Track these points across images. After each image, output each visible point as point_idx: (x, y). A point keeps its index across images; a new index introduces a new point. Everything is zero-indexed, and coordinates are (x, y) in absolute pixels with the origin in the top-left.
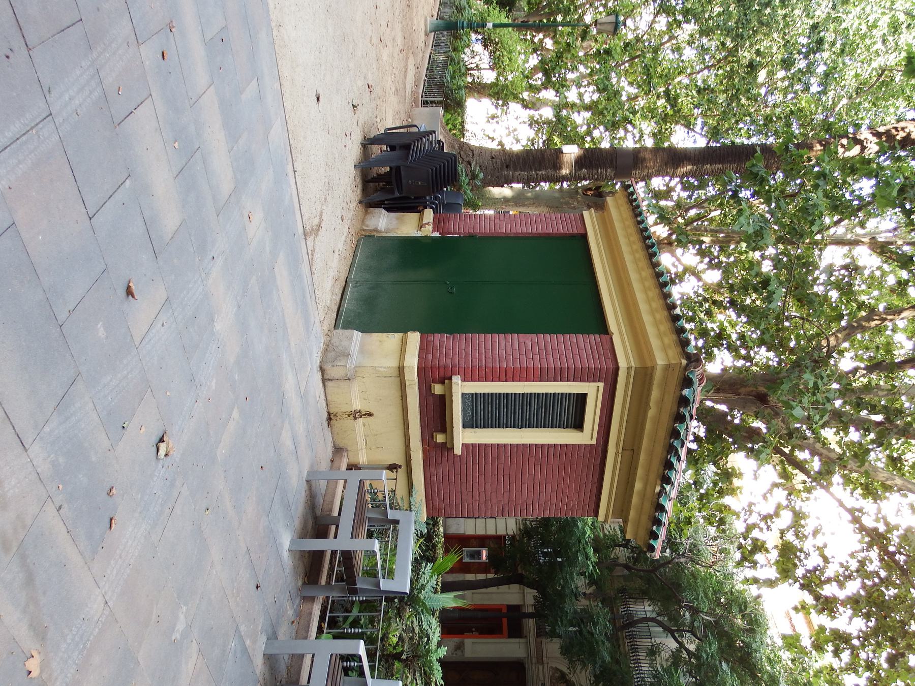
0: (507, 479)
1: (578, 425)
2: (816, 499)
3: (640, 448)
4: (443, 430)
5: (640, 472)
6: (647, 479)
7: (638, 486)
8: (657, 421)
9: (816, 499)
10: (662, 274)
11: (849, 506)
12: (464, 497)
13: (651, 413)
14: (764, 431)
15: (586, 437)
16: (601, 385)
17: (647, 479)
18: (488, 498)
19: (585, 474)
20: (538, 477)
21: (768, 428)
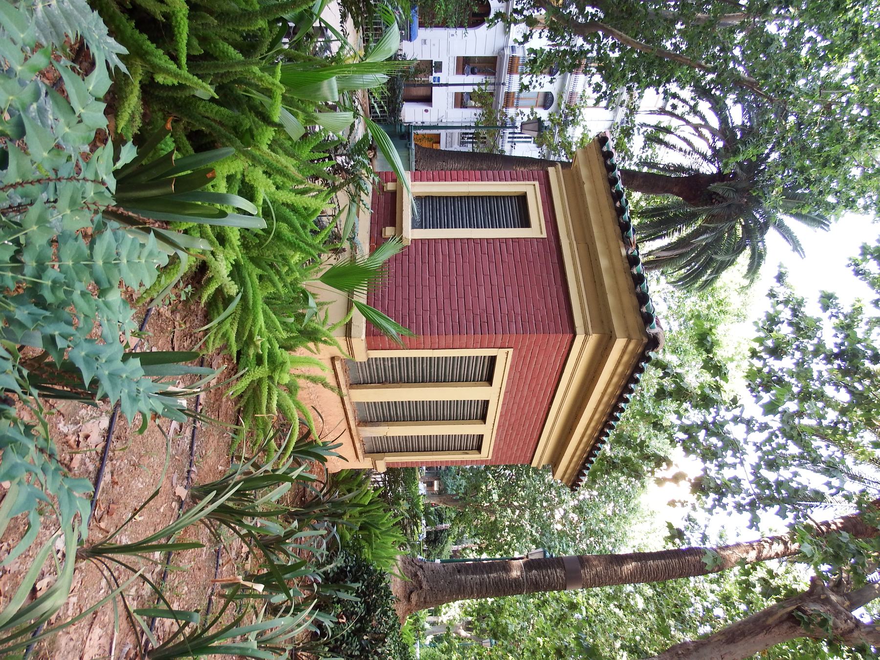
0: (461, 281)
1: (525, 223)
2: (859, 301)
3: (592, 236)
4: (393, 224)
5: (599, 246)
6: (610, 252)
7: (604, 263)
8: (595, 193)
9: (859, 301)
10: (637, 381)
11: (670, 477)
12: (413, 306)
13: (587, 187)
14: (738, 138)
15: (537, 230)
16: (537, 183)
17: (610, 252)
18: (441, 307)
19: (545, 275)
20: (494, 277)
21: (741, 137)
